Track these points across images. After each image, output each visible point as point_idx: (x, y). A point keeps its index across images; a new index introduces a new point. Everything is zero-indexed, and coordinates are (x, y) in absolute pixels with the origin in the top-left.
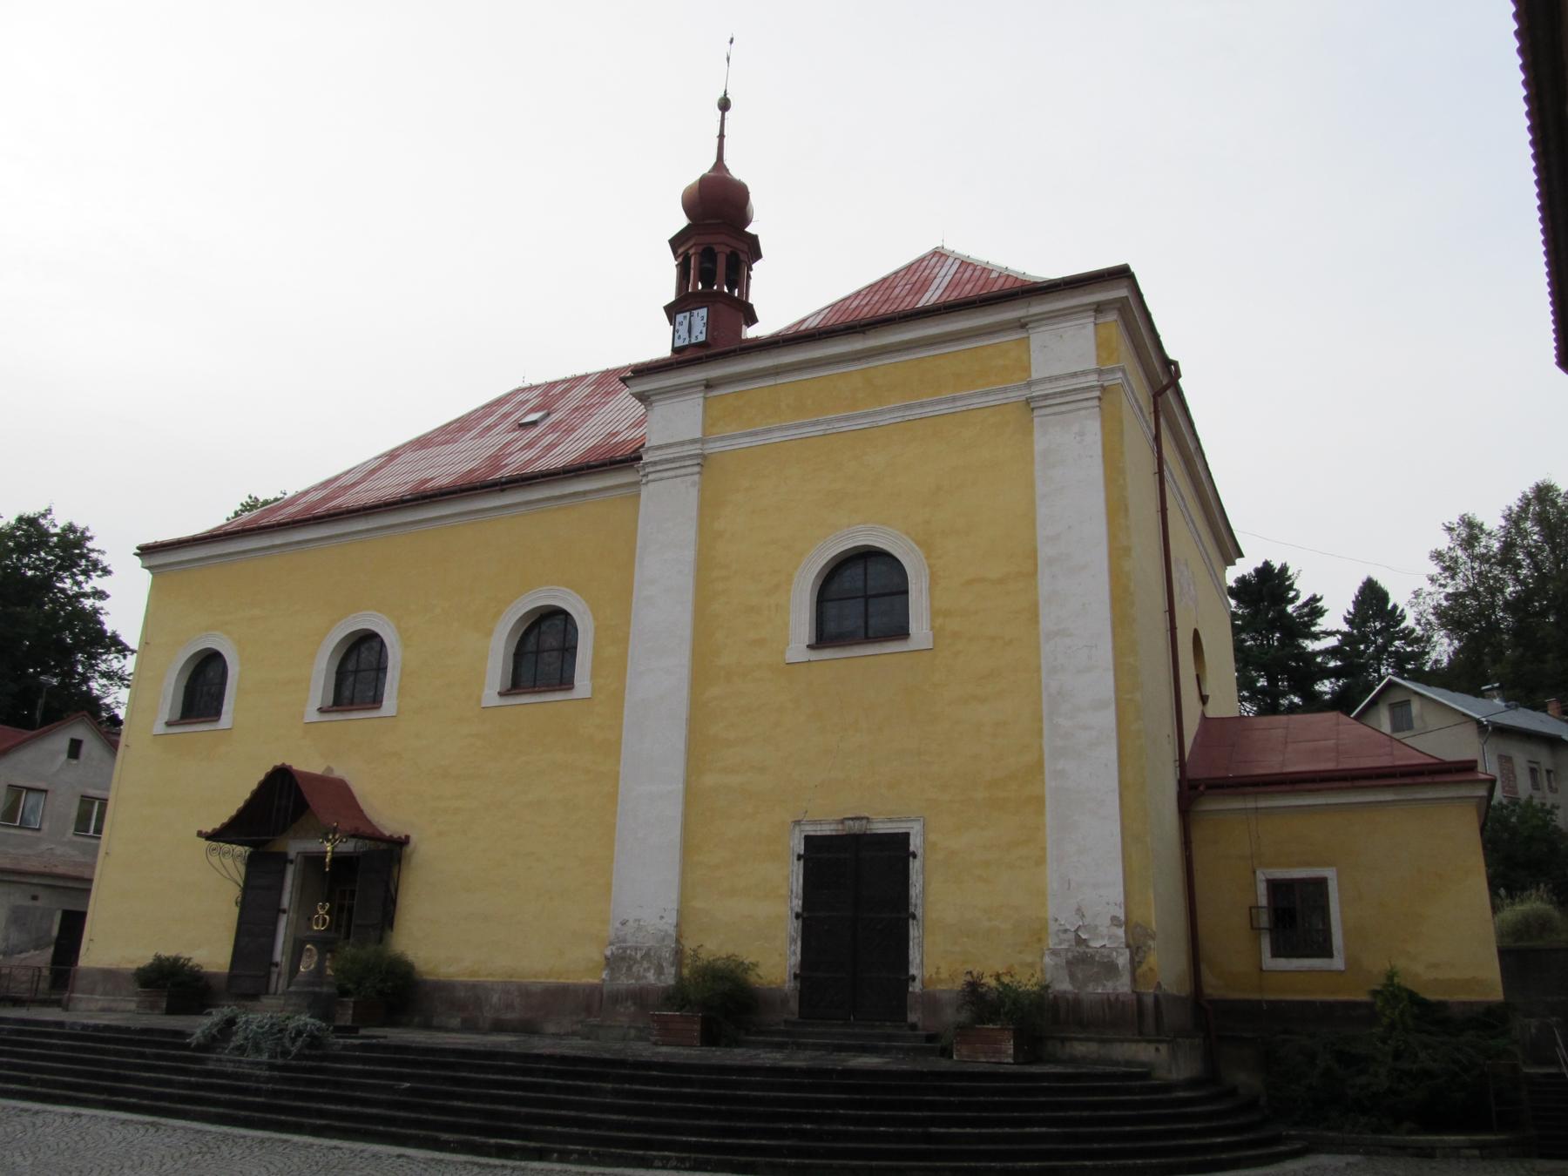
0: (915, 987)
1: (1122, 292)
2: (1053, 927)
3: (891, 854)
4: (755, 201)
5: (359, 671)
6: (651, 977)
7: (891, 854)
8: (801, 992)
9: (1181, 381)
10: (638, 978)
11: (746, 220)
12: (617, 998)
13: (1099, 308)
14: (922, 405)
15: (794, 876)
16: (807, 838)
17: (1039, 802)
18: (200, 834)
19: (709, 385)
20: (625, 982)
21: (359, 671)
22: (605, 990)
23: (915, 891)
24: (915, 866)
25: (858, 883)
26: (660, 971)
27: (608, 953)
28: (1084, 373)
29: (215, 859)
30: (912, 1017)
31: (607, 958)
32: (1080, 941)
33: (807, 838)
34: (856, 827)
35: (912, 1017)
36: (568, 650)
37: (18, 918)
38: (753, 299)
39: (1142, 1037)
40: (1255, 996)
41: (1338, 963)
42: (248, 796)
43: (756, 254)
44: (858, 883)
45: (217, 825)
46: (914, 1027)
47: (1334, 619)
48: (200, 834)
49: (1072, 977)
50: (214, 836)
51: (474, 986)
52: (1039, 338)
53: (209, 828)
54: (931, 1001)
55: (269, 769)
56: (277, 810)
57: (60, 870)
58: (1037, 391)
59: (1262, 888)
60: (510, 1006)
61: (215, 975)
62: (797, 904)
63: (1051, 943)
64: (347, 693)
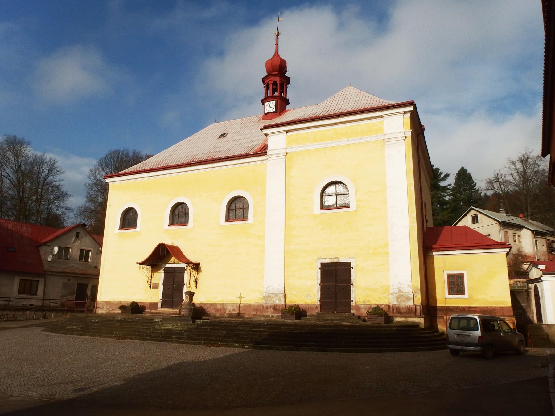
0: (353, 304)
1: (411, 108)
2: (392, 287)
3: (346, 268)
4: (288, 66)
5: (179, 214)
6: (277, 302)
7: (346, 268)
8: (321, 305)
9: (424, 132)
10: (274, 302)
11: (286, 72)
12: (268, 308)
13: (405, 113)
14: (352, 140)
15: (318, 274)
16: (322, 263)
17: (387, 253)
18: (137, 263)
19: (287, 132)
20: (270, 303)
21: (179, 214)
22: (264, 305)
23: (352, 278)
24: (352, 271)
25: (336, 277)
26: (280, 300)
27: (264, 295)
28: (400, 132)
29: (141, 270)
30: (353, 312)
31: (264, 297)
32: (400, 291)
33: (322, 263)
34: (335, 260)
35: (353, 312)
36: (245, 209)
37: (65, 286)
38: (288, 97)
39: (416, 316)
40: (443, 305)
41: (466, 296)
42: (152, 252)
43: (289, 83)
44: (336, 277)
45: (143, 261)
46: (353, 314)
47: (451, 181)
48: (137, 263)
49: (397, 300)
50: (140, 264)
51: (223, 305)
52: (386, 120)
53: (140, 261)
54: (358, 308)
55: (158, 244)
56: (160, 256)
57: (76, 272)
58: (386, 137)
59: (446, 276)
60: (234, 310)
61: (502, 308)
62: (319, 282)
63: (391, 291)
64: (176, 220)
